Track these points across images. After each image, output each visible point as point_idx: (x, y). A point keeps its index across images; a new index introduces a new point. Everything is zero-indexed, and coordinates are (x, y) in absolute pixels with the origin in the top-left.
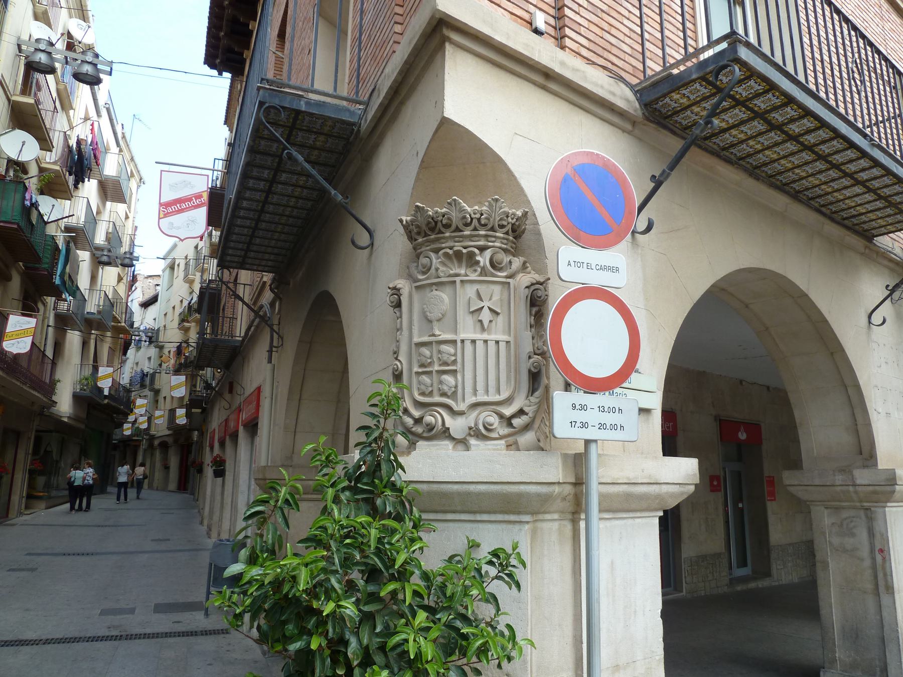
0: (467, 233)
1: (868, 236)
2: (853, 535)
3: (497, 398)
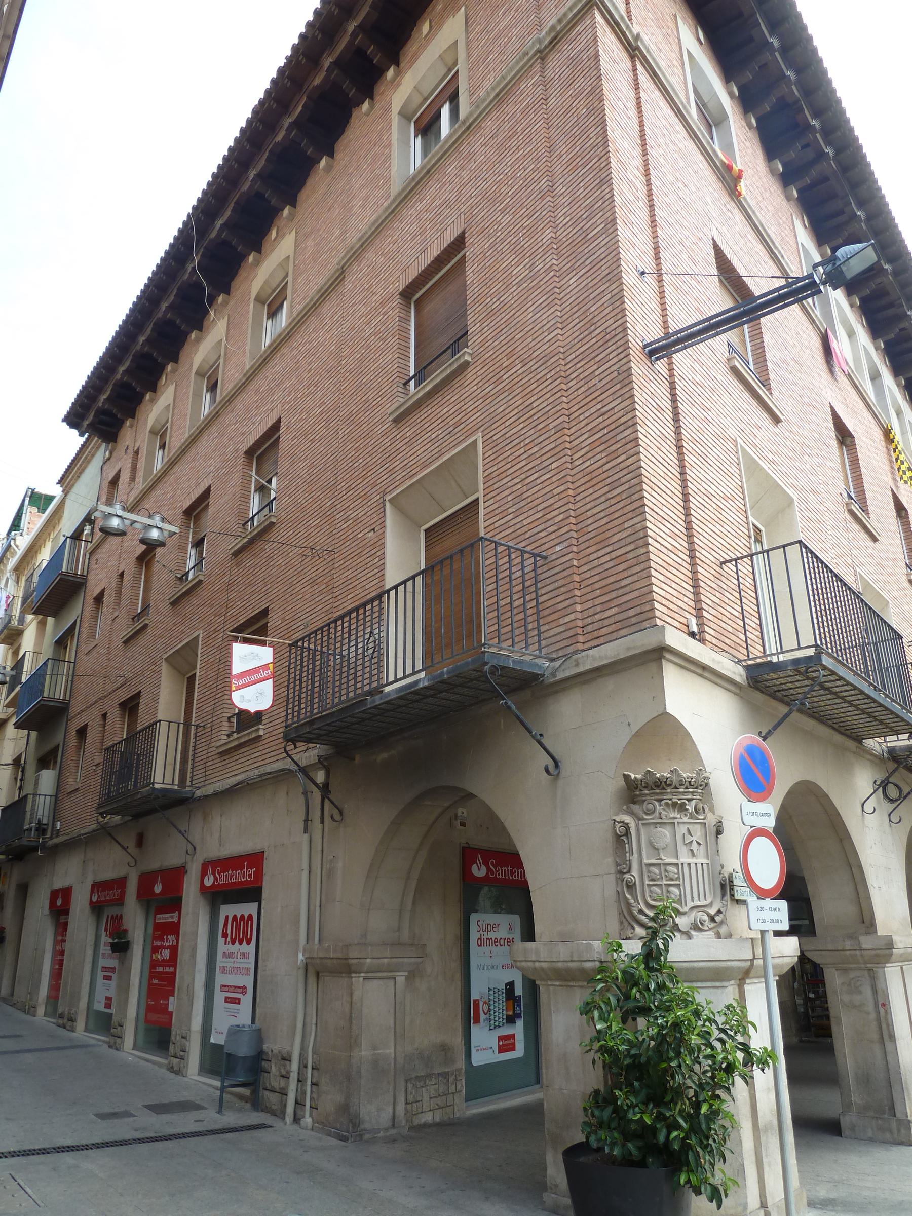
0: (682, 790)
1: (859, 740)
2: (860, 992)
3: (703, 903)
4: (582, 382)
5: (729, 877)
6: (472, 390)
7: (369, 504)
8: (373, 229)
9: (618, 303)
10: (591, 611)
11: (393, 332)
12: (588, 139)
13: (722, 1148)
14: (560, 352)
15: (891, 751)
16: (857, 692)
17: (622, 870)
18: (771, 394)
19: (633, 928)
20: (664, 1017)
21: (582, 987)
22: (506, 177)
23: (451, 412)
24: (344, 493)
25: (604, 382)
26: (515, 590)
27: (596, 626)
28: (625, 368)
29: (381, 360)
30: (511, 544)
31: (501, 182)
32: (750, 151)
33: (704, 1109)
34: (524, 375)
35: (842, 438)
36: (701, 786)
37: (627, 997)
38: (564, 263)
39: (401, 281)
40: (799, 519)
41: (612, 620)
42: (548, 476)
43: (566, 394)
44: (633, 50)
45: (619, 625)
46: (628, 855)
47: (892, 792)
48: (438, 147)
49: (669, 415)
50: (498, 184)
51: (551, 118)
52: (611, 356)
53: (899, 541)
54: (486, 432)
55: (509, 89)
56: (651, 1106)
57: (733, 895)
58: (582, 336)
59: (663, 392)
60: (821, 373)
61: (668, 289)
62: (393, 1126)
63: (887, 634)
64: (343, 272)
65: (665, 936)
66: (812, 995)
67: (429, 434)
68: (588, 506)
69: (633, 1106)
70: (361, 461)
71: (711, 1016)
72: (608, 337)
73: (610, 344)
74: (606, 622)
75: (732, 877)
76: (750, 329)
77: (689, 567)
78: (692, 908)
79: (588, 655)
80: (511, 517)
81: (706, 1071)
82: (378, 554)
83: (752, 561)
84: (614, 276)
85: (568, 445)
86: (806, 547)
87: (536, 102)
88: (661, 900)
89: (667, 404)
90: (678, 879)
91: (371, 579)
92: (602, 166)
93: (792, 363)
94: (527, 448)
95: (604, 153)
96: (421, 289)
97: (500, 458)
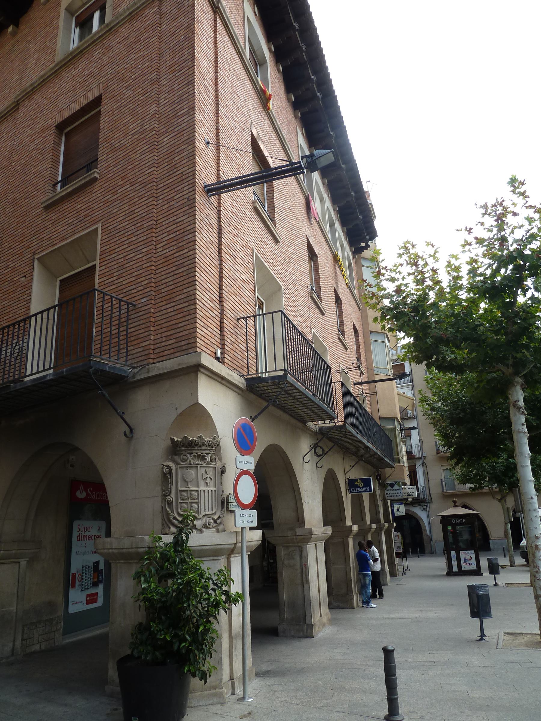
0: (203, 448)
1: (304, 422)
3: (212, 512)
4: (166, 202)
5: (227, 498)
6: (98, 196)
7: (23, 259)
8: (41, 80)
9: (191, 158)
10: (160, 340)
11: (49, 150)
12: (183, 55)
13: (211, 650)
14: (154, 181)
15: (321, 429)
16: (304, 396)
17: (165, 493)
18: (275, 226)
19: (170, 528)
20: (181, 578)
21: (136, 563)
22: (131, 66)
23: (83, 208)
24: (6, 250)
25: (179, 204)
26: (114, 323)
27: (162, 349)
28: (192, 197)
29: (39, 167)
30: (114, 295)
31: (127, 69)
32: (277, 85)
33: (201, 629)
34: (131, 192)
35: (312, 256)
36: (215, 446)
37: (162, 567)
38: (162, 127)
39: (57, 118)
40: (284, 298)
41: (171, 347)
42: (140, 256)
43: (156, 207)
44: (216, 8)
45: (175, 350)
46: (169, 485)
47: (319, 451)
48: (89, 37)
49: (215, 230)
50: (126, 70)
51: (162, 36)
52: (185, 189)
53: (335, 316)
54: (104, 224)
55: (138, 12)
56: (171, 630)
57: (228, 508)
58: (168, 174)
59: (213, 215)
60: (304, 219)
61: (222, 155)
62: (12, 655)
63: (323, 366)
64: (18, 104)
65: (187, 532)
66: (272, 561)
67: (67, 220)
68: (163, 277)
69: (160, 631)
70: (20, 230)
71: (209, 576)
72: (184, 177)
73: (184, 181)
74: (168, 348)
75: (228, 497)
76: (267, 187)
77: (219, 319)
78: (204, 516)
79: (155, 367)
80: (115, 278)
81: (205, 607)
82: (27, 292)
83: (255, 318)
84: (191, 141)
85: (154, 239)
86: (284, 315)
87: (154, 24)
88: (187, 511)
89: (215, 223)
90: (197, 499)
91: (21, 308)
92: (190, 73)
93: (288, 210)
94: (129, 237)
95: (192, 65)
96: (70, 126)
97: (112, 241)
